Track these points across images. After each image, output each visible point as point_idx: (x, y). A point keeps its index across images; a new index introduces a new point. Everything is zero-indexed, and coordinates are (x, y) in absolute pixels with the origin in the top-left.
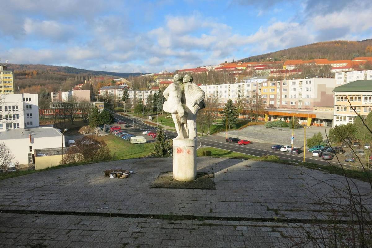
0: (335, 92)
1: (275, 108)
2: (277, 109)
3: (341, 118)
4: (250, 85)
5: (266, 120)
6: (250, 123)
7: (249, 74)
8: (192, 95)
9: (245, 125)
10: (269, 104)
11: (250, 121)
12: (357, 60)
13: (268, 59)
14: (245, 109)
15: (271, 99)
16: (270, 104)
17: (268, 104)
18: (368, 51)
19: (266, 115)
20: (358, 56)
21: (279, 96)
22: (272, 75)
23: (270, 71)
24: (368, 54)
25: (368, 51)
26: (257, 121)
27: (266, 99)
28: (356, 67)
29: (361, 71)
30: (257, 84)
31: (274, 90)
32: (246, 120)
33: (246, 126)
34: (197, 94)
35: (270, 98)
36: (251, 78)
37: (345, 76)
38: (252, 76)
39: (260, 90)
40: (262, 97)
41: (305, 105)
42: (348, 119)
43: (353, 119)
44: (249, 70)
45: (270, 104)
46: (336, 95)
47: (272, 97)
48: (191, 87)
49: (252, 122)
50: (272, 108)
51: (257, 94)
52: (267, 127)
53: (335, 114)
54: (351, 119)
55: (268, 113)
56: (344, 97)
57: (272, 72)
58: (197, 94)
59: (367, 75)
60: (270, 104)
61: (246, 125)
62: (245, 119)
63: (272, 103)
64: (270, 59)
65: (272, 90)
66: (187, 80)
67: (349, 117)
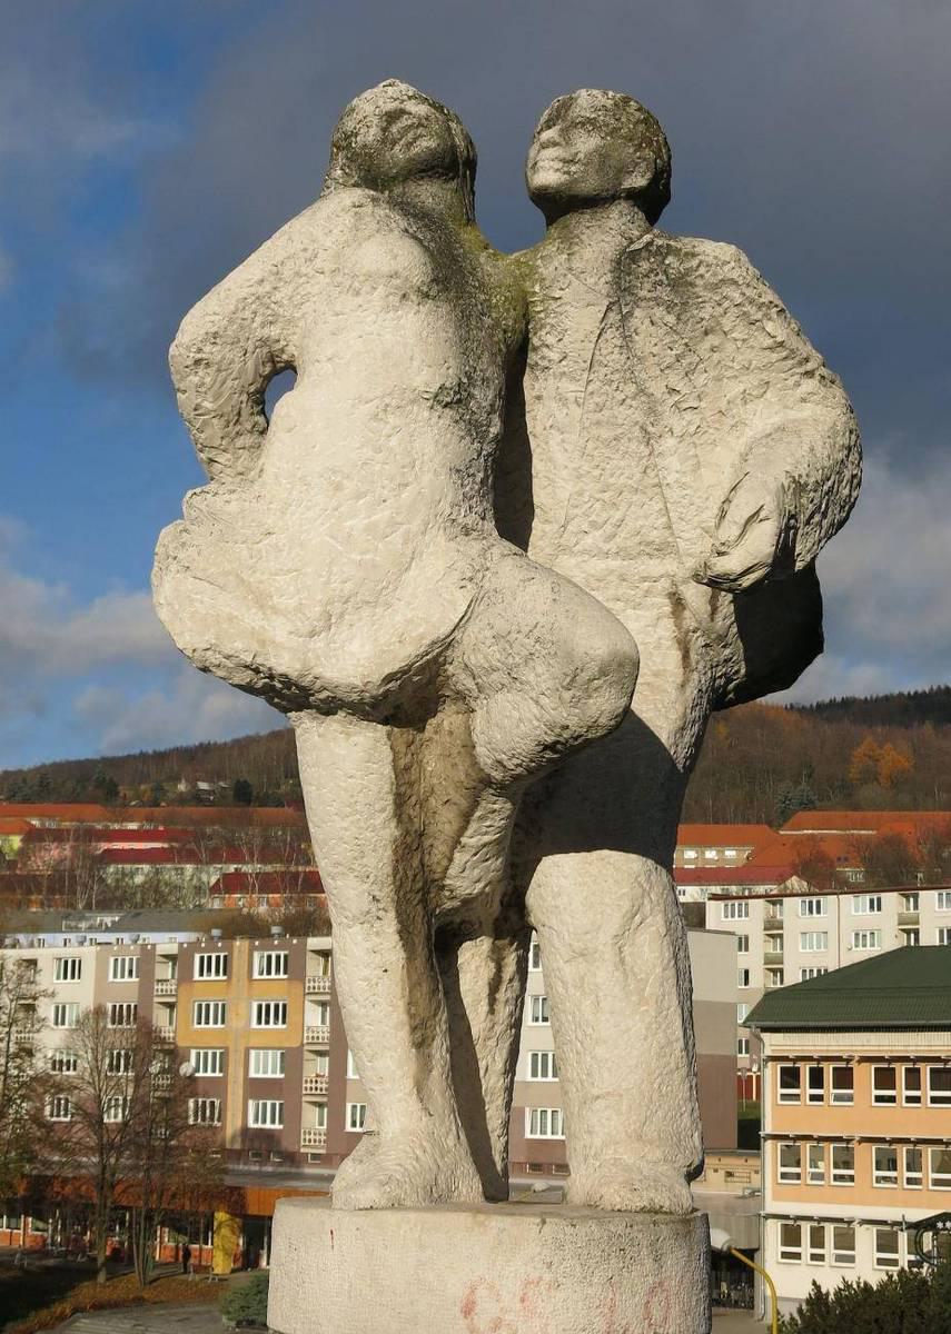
0: (765, 1030)
1: (292, 1158)
2: (308, 1171)
3: (817, 1240)
4: (89, 969)
5: (221, 1265)
6: (86, 1292)
7: (52, 890)
8: (678, 423)
9: (45, 1304)
10: (239, 1124)
11: (89, 1273)
12: (805, 830)
13: (182, 787)
14: (47, 1164)
15: (258, 1088)
16: (245, 1131)
17: (232, 1126)
18: (870, 776)
19: (221, 1216)
20: (808, 805)
21: (322, 1066)
22: (239, 900)
23: (212, 876)
24: (867, 792)
25: (870, 776)
26: (152, 1274)
27: (219, 1086)
28: (822, 877)
29: (875, 896)
30: (147, 956)
31: (282, 1013)
32: (51, 1262)
33: (62, 1318)
34: (762, 417)
35: (252, 1074)
36: (67, 917)
37: (774, 929)
38: (72, 905)
39: (171, 1006)
40: (186, 1069)
41: (528, 1135)
42: (866, 1239)
43: (903, 1238)
44: (52, 855)
45: (251, 1124)
46: (768, 1052)
47: (265, 1066)
48: (680, 283)
49: (102, 1277)
50: (263, 1158)
51: (148, 1034)
52: (239, 1324)
53: (772, 1206)
54: (886, 1243)
55: (242, 1197)
56: (829, 1070)
57: (232, 883)
58: (762, 417)
59: (917, 923)
60: (245, 1131)
61: (57, 1309)
62: (41, 1251)
63: (258, 1116)
64: (203, 786)
65: (264, 1014)
66: (602, 158)
67: (874, 1229)
